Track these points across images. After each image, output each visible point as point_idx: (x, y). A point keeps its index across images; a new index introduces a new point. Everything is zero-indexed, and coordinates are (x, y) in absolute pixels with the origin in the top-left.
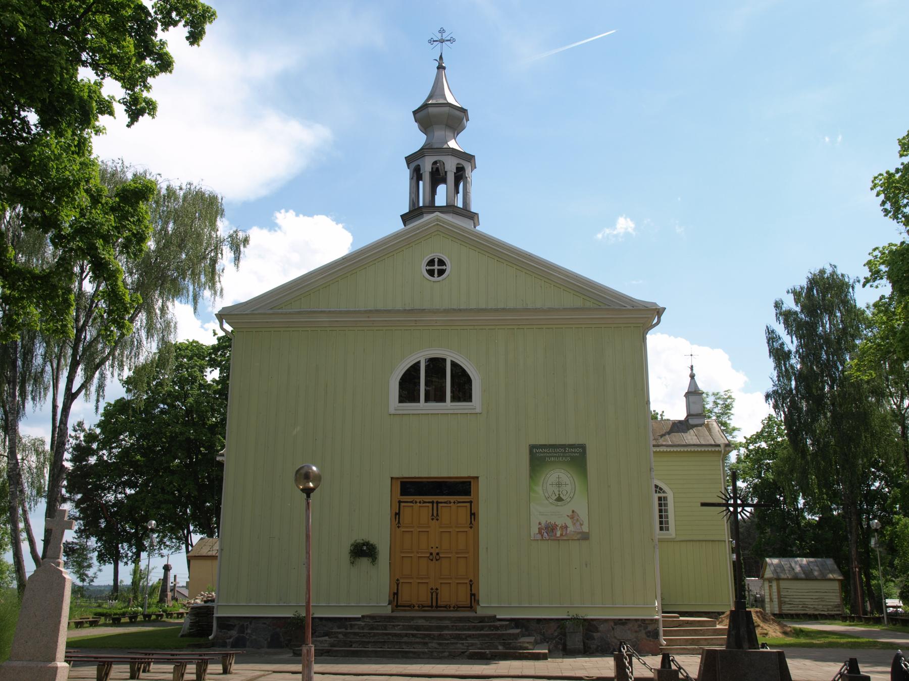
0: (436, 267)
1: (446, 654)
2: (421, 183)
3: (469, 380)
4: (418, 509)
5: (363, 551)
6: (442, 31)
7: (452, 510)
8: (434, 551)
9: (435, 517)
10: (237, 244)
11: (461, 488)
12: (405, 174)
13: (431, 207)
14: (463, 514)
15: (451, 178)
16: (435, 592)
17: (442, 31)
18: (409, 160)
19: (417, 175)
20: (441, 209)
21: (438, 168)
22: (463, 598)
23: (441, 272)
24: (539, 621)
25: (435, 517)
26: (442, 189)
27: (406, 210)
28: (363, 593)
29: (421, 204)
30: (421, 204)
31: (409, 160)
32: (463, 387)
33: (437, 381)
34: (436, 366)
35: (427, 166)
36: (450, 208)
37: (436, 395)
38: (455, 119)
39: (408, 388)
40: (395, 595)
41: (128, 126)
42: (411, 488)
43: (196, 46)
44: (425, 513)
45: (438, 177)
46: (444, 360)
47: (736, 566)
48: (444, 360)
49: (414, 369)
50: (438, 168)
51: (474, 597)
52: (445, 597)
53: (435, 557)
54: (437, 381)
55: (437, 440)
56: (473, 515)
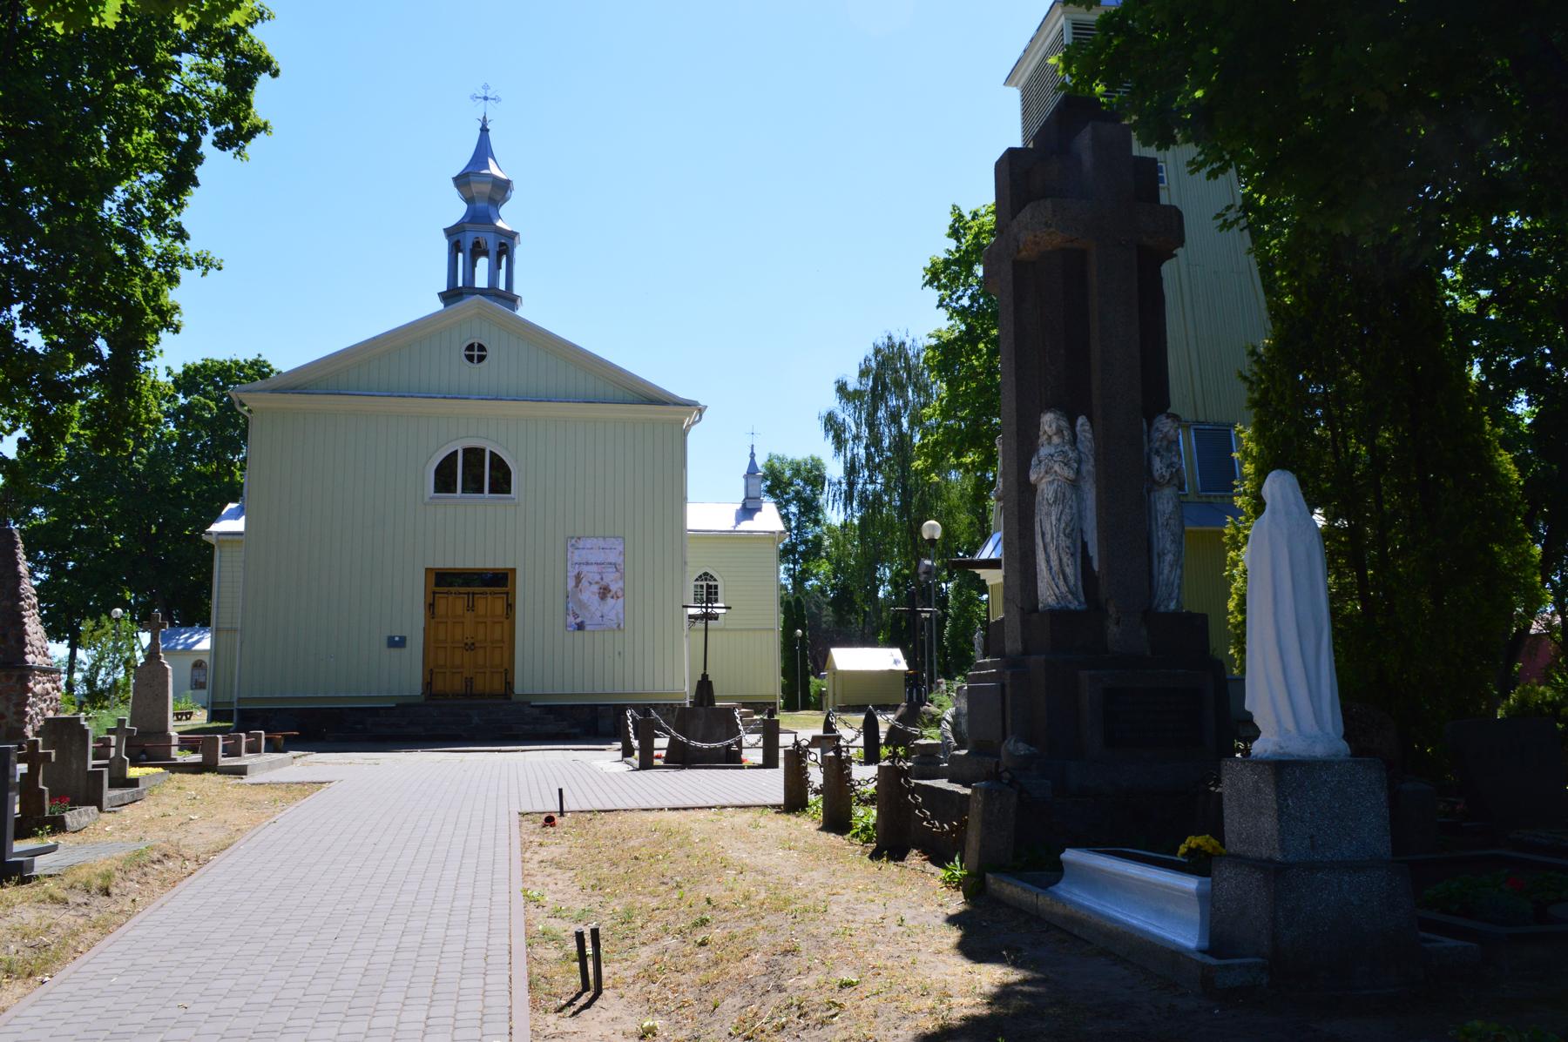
0: (476, 353)
1: (506, 622)
2: (460, 256)
3: (508, 473)
4: (453, 603)
5: (397, 643)
6: (486, 87)
7: (489, 604)
8: (469, 641)
9: (471, 607)
10: (102, 708)
11: (500, 580)
12: (443, 245)
13: (470, 289)
14: (499, 606)
15: (493, 253)
16: (469, 681)
17: (486, 87)
18: (449, 232)
19: (455, 248)
20: (482, 292)
21: (479, 236)
22: (497, 685)
23: (481, 348)
24: (573, 706)
25: (471, 607)
26: (483, 264)
27: (444, 289)
28: (404, 676)
29: (460, 284)
30: (460, 284)
31: (449, 232)
32: (502, 482)
33: (475, 472)
34: (474, 456)
35: (468, 243)
36: (491, 292)
37: (473, 485)
38: (502, 189)
39: (444, 479)
40: (428, 685)
41: (275, 74)
42: (443, 579)
43: (230, 153)
44: (460, 605)
45: (477, 251)
46: (483, 450)
47: (794, 610)
48: (483, 450)
49: (451, 459)
50: (479, 236)
51: (509, 685)
52: (480, 684)
53: (471, 647)
54: (475, 472)
55: (472, 532)
56: (510, 607)
